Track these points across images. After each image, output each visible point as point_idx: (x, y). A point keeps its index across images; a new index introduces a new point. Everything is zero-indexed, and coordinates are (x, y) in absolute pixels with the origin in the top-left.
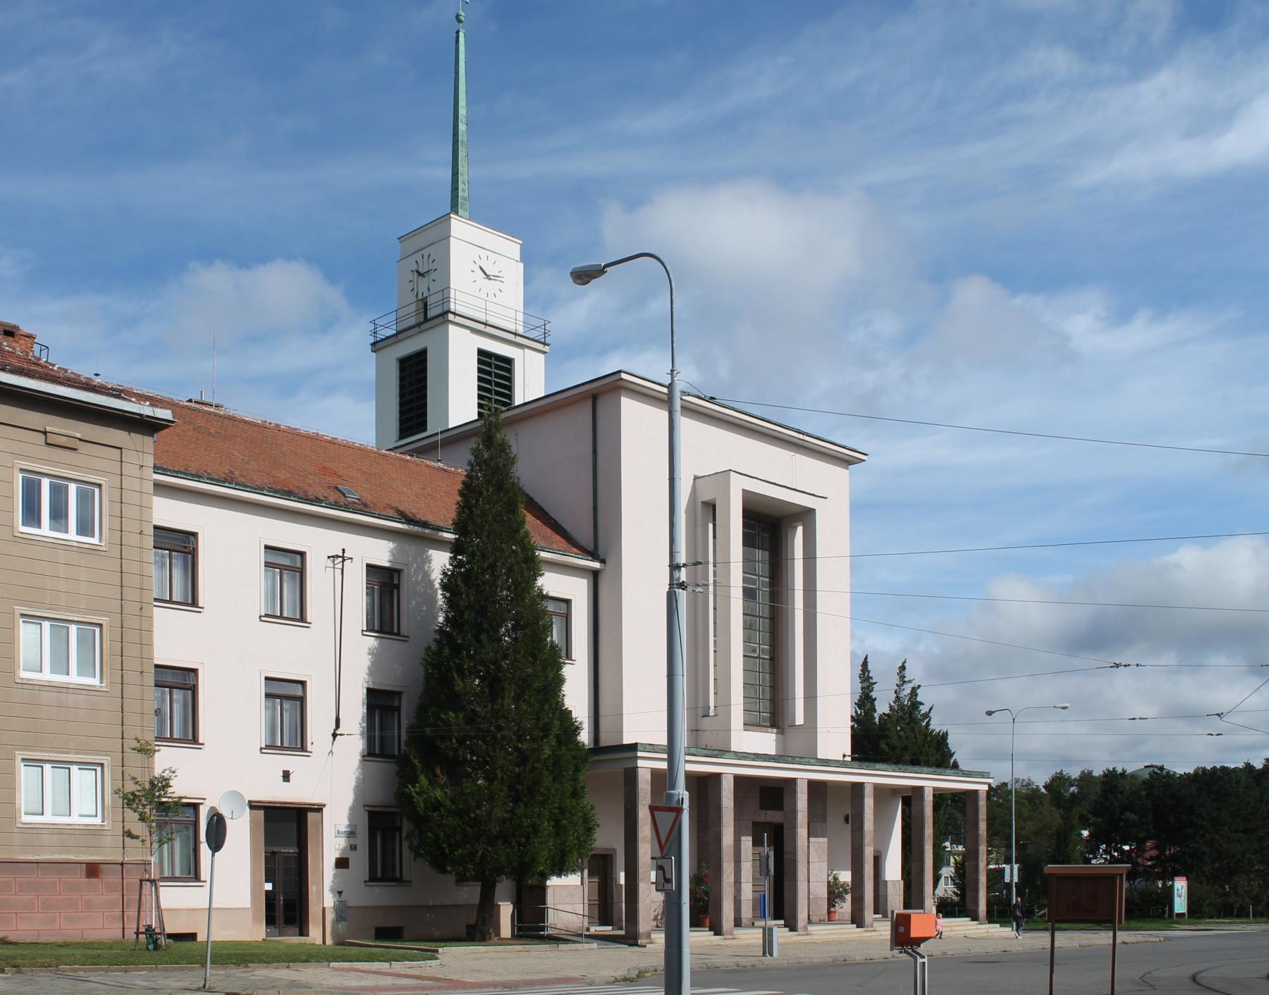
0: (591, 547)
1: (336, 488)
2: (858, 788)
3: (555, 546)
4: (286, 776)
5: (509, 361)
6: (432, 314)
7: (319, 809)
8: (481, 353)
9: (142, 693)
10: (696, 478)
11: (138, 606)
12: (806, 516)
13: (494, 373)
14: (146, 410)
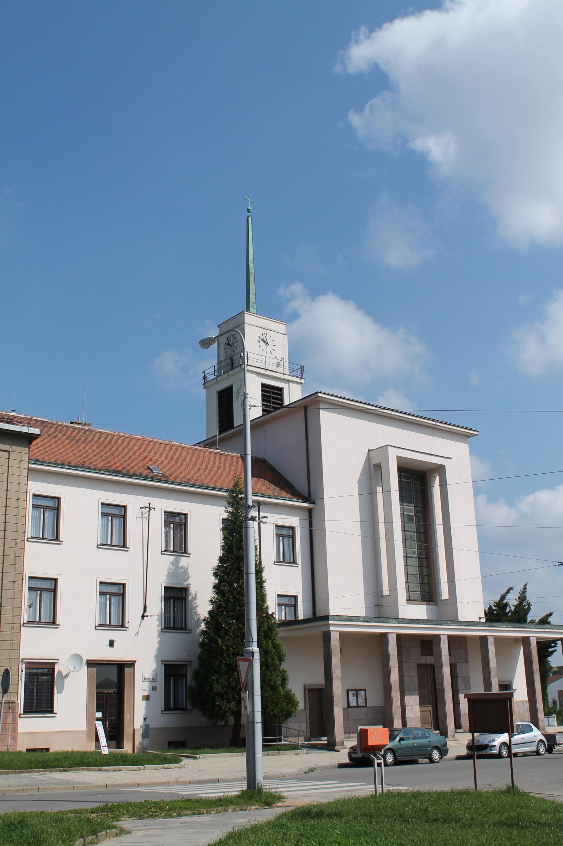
0: (306, 494)
1: (149, 468)
2: (483, 640)
4: (112, 643)
5: (281, 390)
7: (131, 664)
8: (263, 385)
9: (14, 595)
10: (369, 451)
11: (14, 542)
12: (440, 470)
13: (272, 396)
14: (25, 429)
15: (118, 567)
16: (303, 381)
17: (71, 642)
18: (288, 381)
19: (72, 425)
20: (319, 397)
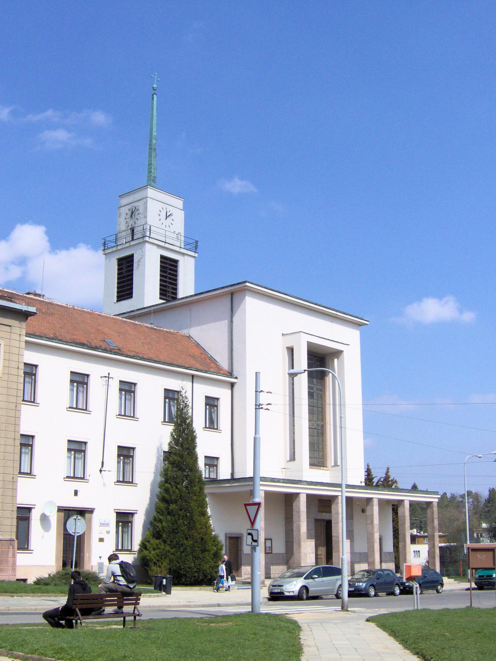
2: (369, 500)
3: (212, 370)
4: (76, 493)
5: (176, 261)
6: (136, 235)
8: (162, 257)
13: (169, 269)
14: (24, 307)
15: (80, 427)
16: (196, 255)
17: (45, 490)
18: (184, 254)
19: (28, 296)
20: (247, 286)
